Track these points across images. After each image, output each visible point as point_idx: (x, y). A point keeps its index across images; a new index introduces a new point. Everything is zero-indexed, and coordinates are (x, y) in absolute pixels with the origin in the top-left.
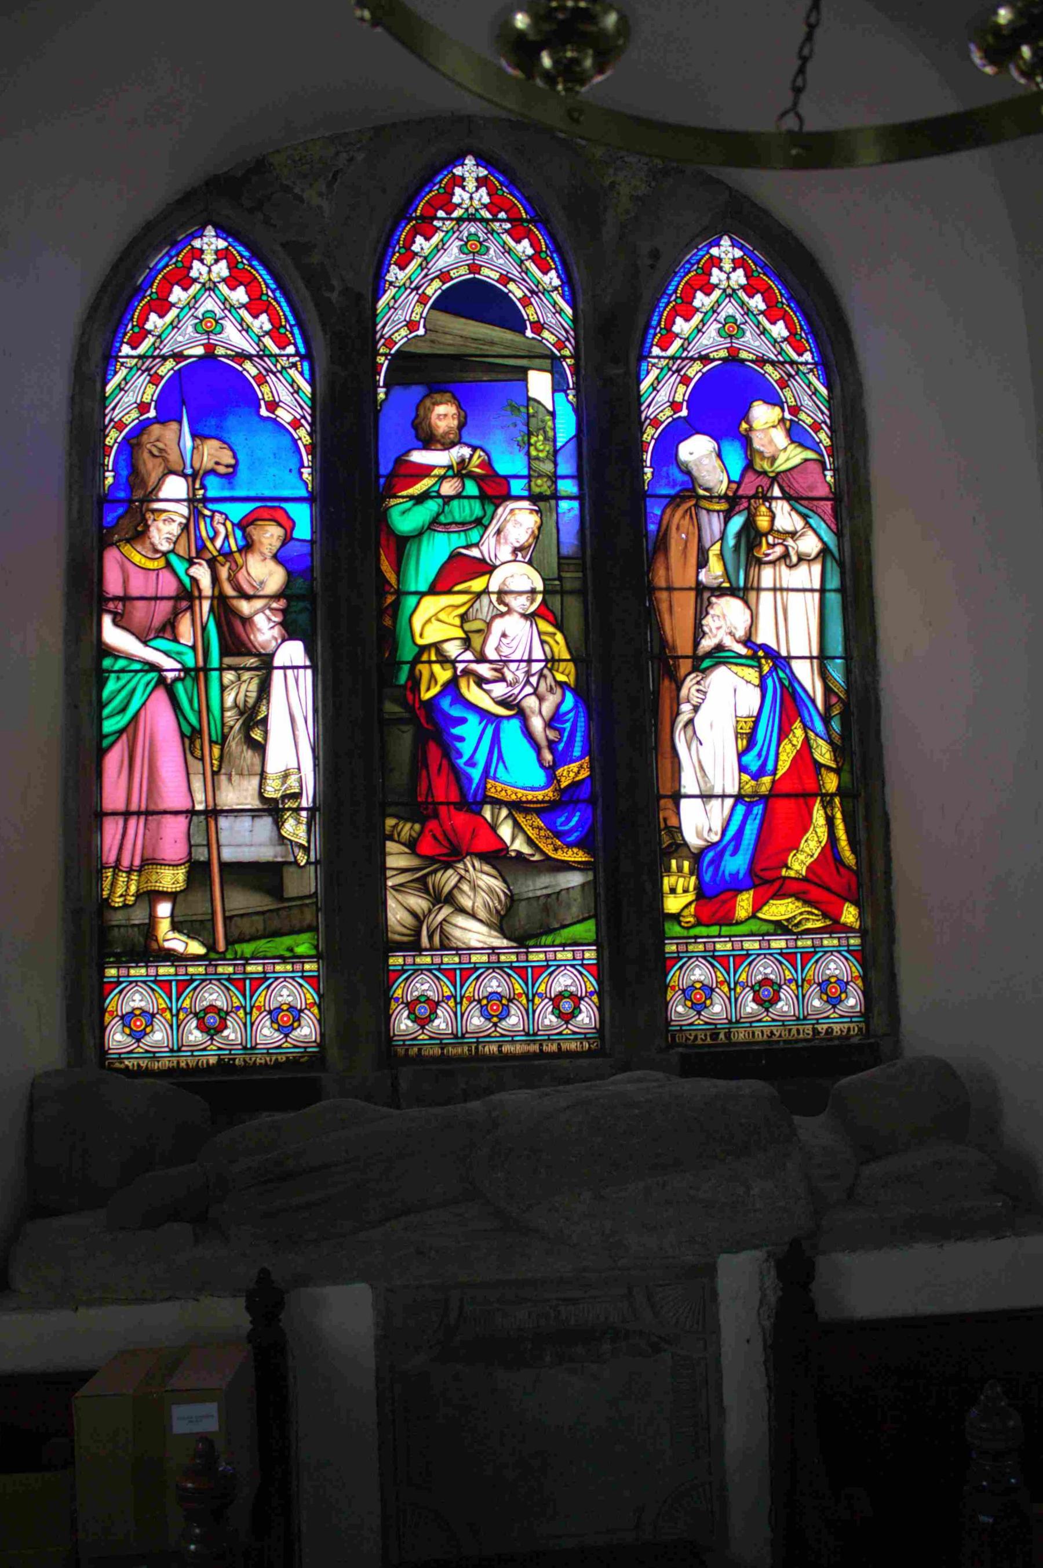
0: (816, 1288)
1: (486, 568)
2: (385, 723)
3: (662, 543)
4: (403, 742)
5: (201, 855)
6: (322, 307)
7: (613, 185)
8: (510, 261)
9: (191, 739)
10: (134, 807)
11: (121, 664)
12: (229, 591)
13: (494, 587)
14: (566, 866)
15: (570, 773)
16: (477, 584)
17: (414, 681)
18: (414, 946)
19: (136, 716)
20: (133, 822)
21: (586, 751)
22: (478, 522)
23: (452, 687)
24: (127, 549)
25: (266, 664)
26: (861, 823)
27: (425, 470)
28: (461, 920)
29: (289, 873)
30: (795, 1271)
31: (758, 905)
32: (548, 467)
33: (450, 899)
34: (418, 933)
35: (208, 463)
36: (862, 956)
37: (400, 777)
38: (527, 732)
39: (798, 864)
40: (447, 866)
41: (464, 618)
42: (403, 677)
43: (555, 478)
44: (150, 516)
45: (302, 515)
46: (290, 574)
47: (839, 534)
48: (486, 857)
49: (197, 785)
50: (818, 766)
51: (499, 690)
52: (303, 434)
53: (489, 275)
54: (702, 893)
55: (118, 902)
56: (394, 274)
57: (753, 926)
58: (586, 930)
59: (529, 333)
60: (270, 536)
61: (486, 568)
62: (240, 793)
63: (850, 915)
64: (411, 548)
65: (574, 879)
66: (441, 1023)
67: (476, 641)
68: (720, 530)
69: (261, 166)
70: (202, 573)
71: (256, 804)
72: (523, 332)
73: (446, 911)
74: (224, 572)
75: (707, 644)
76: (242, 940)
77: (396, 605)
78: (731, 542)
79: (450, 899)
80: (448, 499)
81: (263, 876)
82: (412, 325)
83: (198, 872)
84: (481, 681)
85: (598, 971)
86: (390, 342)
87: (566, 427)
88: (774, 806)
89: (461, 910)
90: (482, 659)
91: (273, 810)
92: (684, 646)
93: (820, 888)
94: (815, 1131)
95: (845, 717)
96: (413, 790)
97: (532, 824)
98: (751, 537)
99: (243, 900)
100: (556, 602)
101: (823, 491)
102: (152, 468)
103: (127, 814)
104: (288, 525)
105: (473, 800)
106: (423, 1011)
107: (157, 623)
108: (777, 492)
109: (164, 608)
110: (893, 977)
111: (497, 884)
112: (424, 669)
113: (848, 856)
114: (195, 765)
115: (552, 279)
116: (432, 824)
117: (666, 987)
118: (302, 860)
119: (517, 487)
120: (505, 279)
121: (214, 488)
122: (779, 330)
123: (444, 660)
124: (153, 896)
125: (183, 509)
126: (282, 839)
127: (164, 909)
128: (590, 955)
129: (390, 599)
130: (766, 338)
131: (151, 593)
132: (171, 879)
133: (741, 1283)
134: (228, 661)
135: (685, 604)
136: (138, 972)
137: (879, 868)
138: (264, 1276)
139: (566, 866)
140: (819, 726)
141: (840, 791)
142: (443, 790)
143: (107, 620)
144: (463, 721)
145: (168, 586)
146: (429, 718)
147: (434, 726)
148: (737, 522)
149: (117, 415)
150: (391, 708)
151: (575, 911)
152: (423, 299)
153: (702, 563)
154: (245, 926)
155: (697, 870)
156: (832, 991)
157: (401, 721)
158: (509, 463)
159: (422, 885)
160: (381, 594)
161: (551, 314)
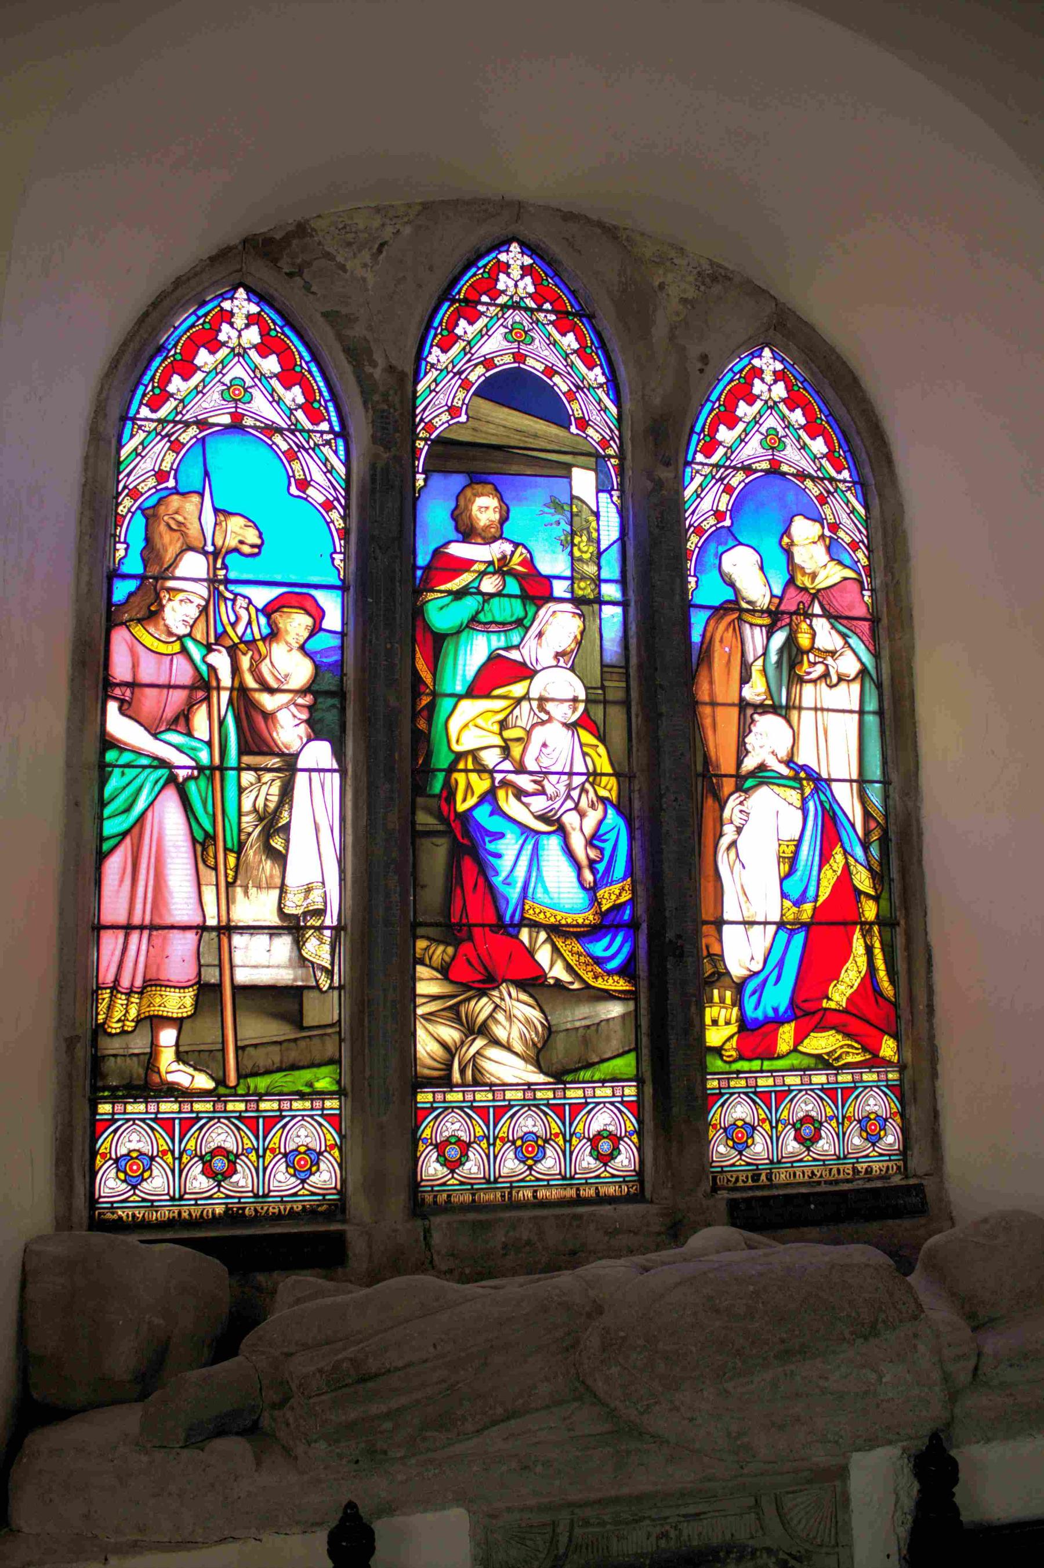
1: (525, 672)
2: (416, 835)
4: (436, 856)
5: (211, 976)
6: (366, 388)
7: (662, 286)
8: (552, 351)
9: (203, 846)
10: (137, 920)
12: (250, 682)
13: (534, 694)
14: (608, 996)
15: (611, 895)
16: (517, 689)
17: (449, 790)
18: (445, 1082)
20: (135, 937)
21: (629, 871)
22: (519, 623)
23: (489, 797)
24: (138, 630)
25: (290, 765)
26: (900, 954)
27: (466, 565)
28: (493, 1052)
29: (309, 997)
30: (935, 1469)
31: (799, 1039)
33: (483, 1030)
34: (449, 1067)
35: (232, 542)
36: (898, 1091)
37: (432, 895)
38: (568, 851)
39: (839, 994)
40: (482, 993)
41: (503, 725)
43: (598, 581)
46: (317, 666)
47: (876, 655)
48: (522, 985)
51: (539, 804)
53: (534, 366)
54: (745, 1025)
55: (115, 1027)
57: (794, 1060)
59: (573, 429)
60: (296, 624)
61: (525, 672)
62: (255, 907)
63: (888, 1048)
64: (449, 646)
67: (516, 750)
69: (302, 230)
70: (221, 660)
71: (274, 920)
74: (245, 662)
75: (749, 764)
77: (432, 707)
78: (773, 658)
79: (483, 1030)
80: (488, 597)
81: (282, 1001)
82: (453, 411)
83: (207, 993)
84: (520, 794)
85: (636, 1108)
86: (430, 427)
87: (610, 529)
88: (821, 934)
89: (495, 1042)
90: (521, 770)
92: (727, 765)
93: (864, 1019)
98: (793, 655)
99: (259, 1029)
100: (597, 713)
101: (861, 611)
103: (128, 928)
104: (318, 614)
107: (169, 714)
109: (178, 697)
111: (535, 1014)
112: (460, 778)
113: (885, 985)
114: (208, 876)
115: (597, 375)
118: (324, 983)
119: (560, 588)
121: (238, 567)
122: (819, 446)
123: (481, 769)
124: (155, 1022)
126: (302, 961)
127: (168, 1036)
128: (630, 1092)
129: (425, 700)
130: (806, 452)
131: (163, 680)
132: (177, 1003)
133: (877, 1489)
134: (247, 759)
140: (859, 852)
141: (879, 920)
142: (479, 913)
143: (112, 707)
145: (182, 673)
147: (468, 844)
148: (779, 638)
150: (424, 819)
151: (615, 1044)
153: (745, 679)
154: (261, 1058)
155: (738, 1002)
158: (552, 562)
159: (454, 1014)
160: (416, 695)
161: (598, 414)
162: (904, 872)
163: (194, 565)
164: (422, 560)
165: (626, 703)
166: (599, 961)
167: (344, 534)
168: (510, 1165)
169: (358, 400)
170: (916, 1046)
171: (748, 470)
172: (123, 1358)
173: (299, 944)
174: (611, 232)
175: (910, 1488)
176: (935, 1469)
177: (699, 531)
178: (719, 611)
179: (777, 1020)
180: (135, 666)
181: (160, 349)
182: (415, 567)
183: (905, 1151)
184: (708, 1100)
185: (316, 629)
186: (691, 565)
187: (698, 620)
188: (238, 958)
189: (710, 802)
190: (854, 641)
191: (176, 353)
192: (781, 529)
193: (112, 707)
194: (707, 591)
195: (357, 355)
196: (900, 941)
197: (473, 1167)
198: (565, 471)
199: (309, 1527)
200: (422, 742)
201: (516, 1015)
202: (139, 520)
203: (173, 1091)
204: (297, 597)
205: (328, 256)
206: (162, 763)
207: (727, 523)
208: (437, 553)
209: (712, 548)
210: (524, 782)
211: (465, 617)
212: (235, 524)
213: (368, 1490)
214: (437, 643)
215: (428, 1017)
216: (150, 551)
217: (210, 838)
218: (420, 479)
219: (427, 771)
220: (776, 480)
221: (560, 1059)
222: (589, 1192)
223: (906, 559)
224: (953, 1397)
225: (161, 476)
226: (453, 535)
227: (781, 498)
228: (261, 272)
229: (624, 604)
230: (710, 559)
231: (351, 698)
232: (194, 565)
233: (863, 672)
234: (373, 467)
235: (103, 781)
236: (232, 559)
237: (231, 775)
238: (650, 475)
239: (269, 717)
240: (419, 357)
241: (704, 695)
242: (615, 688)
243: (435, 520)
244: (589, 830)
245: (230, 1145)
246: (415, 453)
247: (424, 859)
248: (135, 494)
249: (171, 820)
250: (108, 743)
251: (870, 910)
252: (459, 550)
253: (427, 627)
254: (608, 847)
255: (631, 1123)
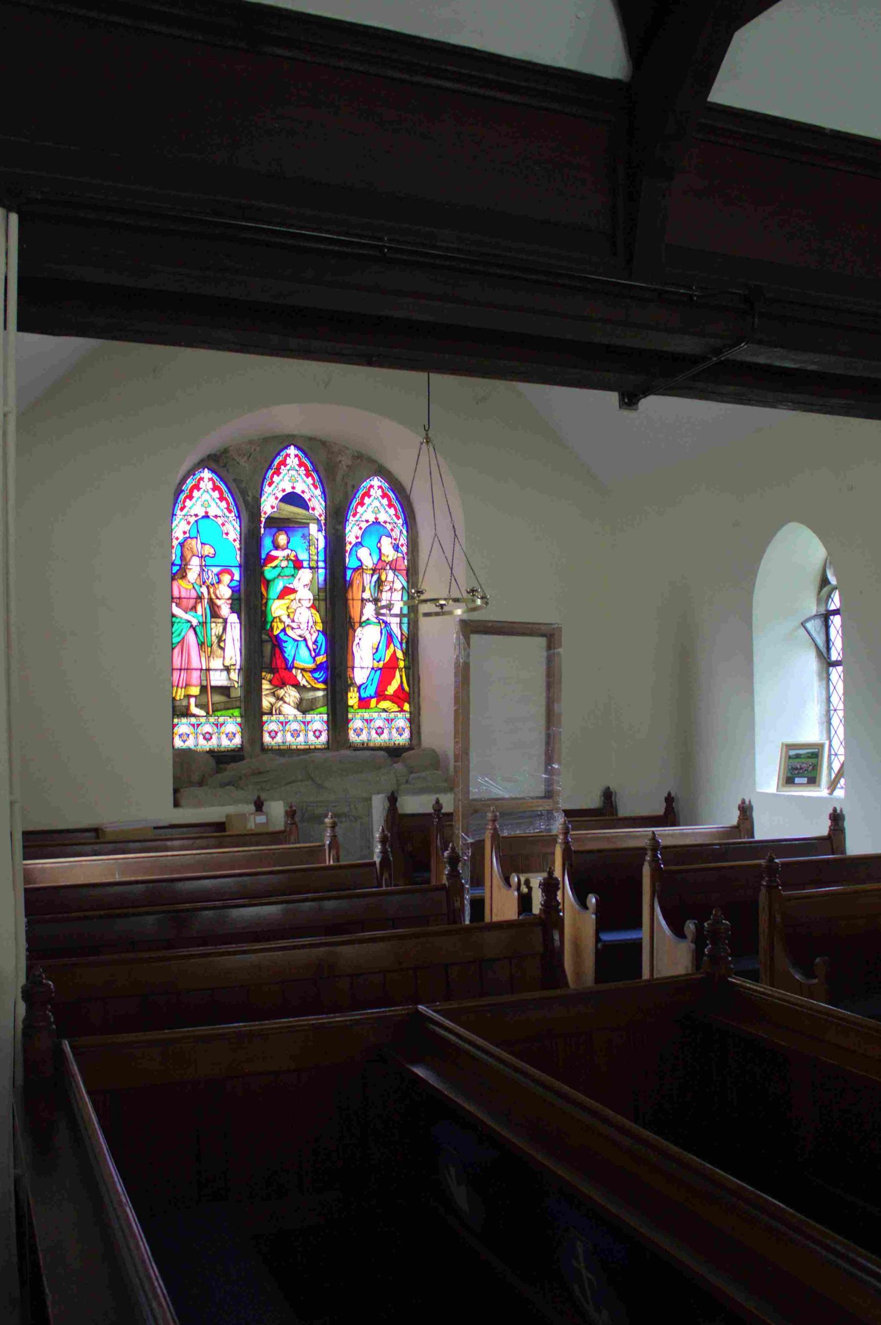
0: (398, 805)
1: (294, 591)
2: (262, 642)
3: (351, 583)
4: (268, 648)
5: (204, 683)
6: (246, 502)
7: (340, 462)
8: (305, 486)
9: (201, 645)
10: (183, 667)
11: (177, 620)
12: (213, 597)
13: (297, 599)
14: (318, 689)
15: (321, 659)
16: (292, 596)
17: (272, 628)
18: (271, 713)
19: (183, 638)
20: (182, 672)
21: (326, 652)
22: (293, 576)
23: (284, 630)
24: (180, 581)
25: (225, 621)
26: (411, 678)
27: (276, 558)
28: (285, 705)
29: (232, 690)
30: (393, 799)
31: (378, 703)
32: (315, 558)
33: (282, 699)
34: (272, 709)
35: (206, 553)
36: (410, 720)
37: (267, 659)
38: (307, 646)
39: (391, 690)
40: (281, 688)
41: (288, 608)
42: (268, 627)
43: (317, 561)
44: (187, 571)
45: (237, 573)
46: (233, 591)
47: (408, 582)
48: (293, 686)
49: (203, 659)
50: (398, 659)
51: (299, 632)
52: (237, 544)
53: (298, 491)
54: (361, 699)
55: (178, 698)
56: (267, 489)
57: (376, 710)
58: (324, 709)
59: (311, 511)
60: (226, 578)
61: (294, 591)
62: (216, 663)
63: (406, 707)
64: (271, 583)
65: (320, 694)
66: (279, 739)
67: (292, 616)
68: (369, 580)
69: (226, 451)
70: (204, 590)
71: (222, 667)
72: (308, 510)
73: (281, 702)
74: (212, 590)
75: (364, 619)
76: (217, 710)
77: (266, 603)
78: (373, 584)
79: (282, 699)
80: (283, 568)
81: (224, 690)
82: (273, 507)
83: (203, 689)
84: (293, 629)
85: (327, 723)
86: (265, 513)
87: (322, 544)
88: (387, 671)
89: (285, 702)
90: (293, 621)
91: (227, 669)
92: (357, 619)
93: (399, 698)
94: (399, 767)
95: (407, 642)
96: (271, 662)
97: (308, 675)
98: (379, 583)
99: (218, 698)
100: (317, 603)
101: (403, 567)
102: (188, 554)
103: (181, 670)
104: (232, 575)
105: (289, 668)
106: (273, 734)
107: (190, 607)
108: (388, 567)
109: (192, 602)
110: (419, 727)
111: (297, 695)
112: (275, 624)
113: (406, 688)
114: (202, 654)
115: (318, 492)
116: (277, 675)
117: (348, 728)
118: (236, 685)
119: (305, 564)
120: (303, 492)
121: (209, 561)
122: (392, 511)
123: (281, 621)
124: (188, 697)
125: (198, 568)
126: (230, 679)
127: (192, 700)
128: (325, 717)
129: (264, 601)
130: (386, 515)
131: (188, 596)
132: (195, 691)
133: (379, 805)
134: (213, 620)
135: (358, 604)
136: (184, 720)
137: (416, 690)
138: (259, 797)
139: (318, 689)
140: (399, 645)
141: (405, 667)
142: (280, 663)
143: (174, 605)
144: (286, 642)
145: (193, 594)
146: (277, 641)
147: (278, 644)
148: (375, 577)
149: (176, 535)
150: (265, 637)
151: (321, 703)
152: (276, 498)
153: (363, 591)
154: (218, 706)
155: (359, 691)
156: (400, 731)
157: (268, 641)
158: (303, 556)
159: (273, 694)
160: (262, 599)
161: (318, 506)
162: (413, 652)
163: (195, 561)
164: (263, 556)
165: (326, 600)
166: (316, 679)
167: (240, 549)
168: (289, 738)
169: (244, 508)
170: (414, 707)
171: (367, 521)
172: (196, 777)
173: (229, 673)
174: (324, 443)
175: (387, 804)
176: (393, 799)
177: (350, 543)
178: (355, 570)
179: (371, 697)
180: (180, 592)
181: (183, 491)
182: (261, 559)
183: (411, 739)
184: (348, 721)
185: (232, 580)
186: (347, 555)
187: (349, 573)
188: (212, 678)
189: (351, 630)
190: (400, 577)
191: (187, 493)
192: (377, 541)
193: (174, 605)
194: (351, 562)
195: (244, 493)
196: (411, 673)
197: (279, 739)
198: (306, 526)
199: (251, 803)
200: (264, 614)
201: (291, 694)
202: (179, 547)
203: (194, 716)
204: (226, 570)
205: (233, 459)
206: (189, 621)
207: (359, 540)
208: (268, 554)
209: (354, 549)
210: (294, 625)
211: (276, 575)
212: (207, 547)
213: (263, 796)
214: (267, 583)
215: (266, 695)
216: (182, 557)
217: (203, 643)
218: (262, 531)
219: (265, 622)
220: (377, 527)
221: (304, 707)
222: (313, 747)
223: (418, 551)
224: (399, 785)
225: (185, 533)
226: (272, 548)
227: (378, 531)
228: (213, 465)
229: (325, 568)
230: (354, 553)
231: (243, 601)
232: (195, 561)
233: (403, 588)
234: (249, 531)
235: (172, 626)
236: (207, 558)
237: (208, 625)
238: (334, 529)
239: (219, 607)
240: (262, 490)
241: (350, 597)
242: (322, 595)
243: (267, 543)
244: (313, 640)
245: (211, 731)
246: (261, 522)
247: (264, 649)
248: (177, 539)
249: (191, 636)
250: (173, 616)
251: (402, 664)
252: (274, 553)
253: (264, 578)
254: (319, 645)
255: (325, 727)
